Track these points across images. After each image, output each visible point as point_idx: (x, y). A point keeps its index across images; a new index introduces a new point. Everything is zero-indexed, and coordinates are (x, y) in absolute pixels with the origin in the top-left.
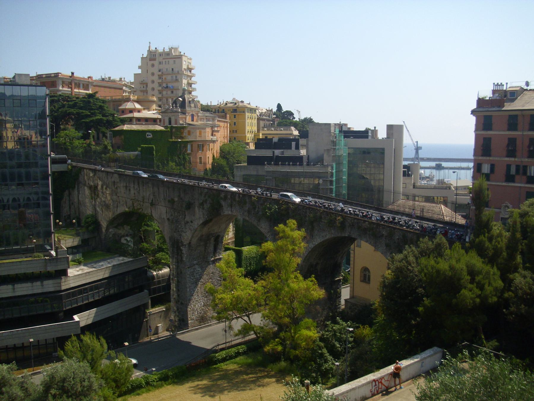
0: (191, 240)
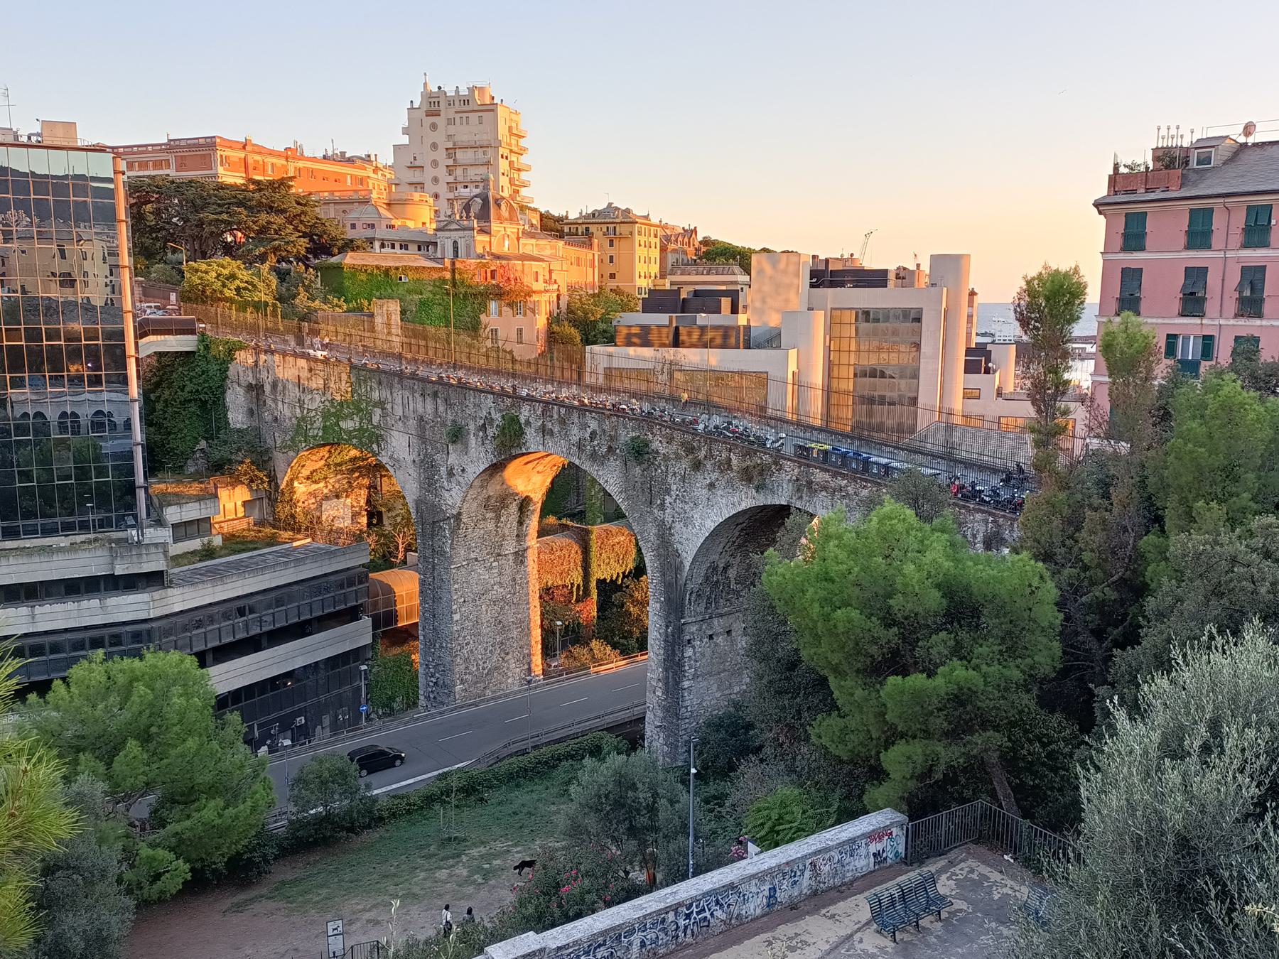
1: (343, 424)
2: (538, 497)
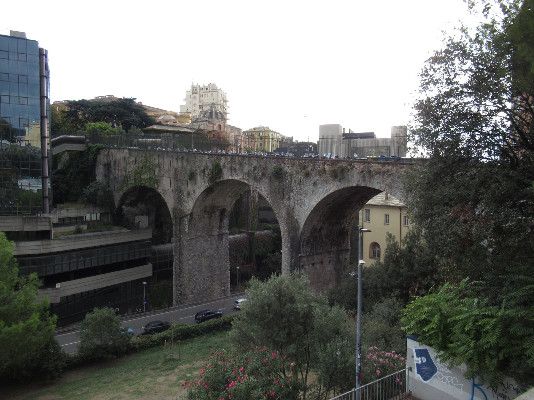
0: (192, 210)
1: (143, 177)
2: (229, 209)
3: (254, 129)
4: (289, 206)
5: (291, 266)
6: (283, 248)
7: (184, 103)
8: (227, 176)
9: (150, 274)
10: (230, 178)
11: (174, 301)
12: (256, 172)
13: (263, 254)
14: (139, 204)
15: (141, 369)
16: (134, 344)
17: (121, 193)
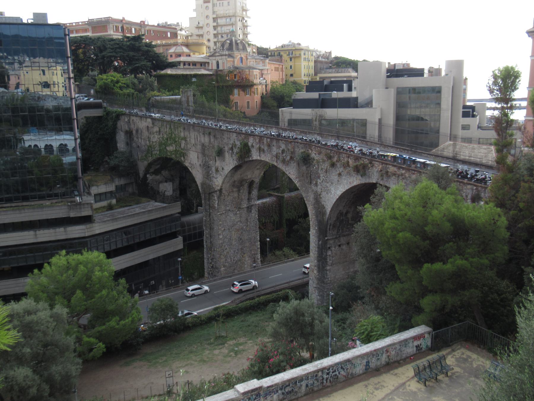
0: (221, 186)
1: (168, 148)
2: (257, 180)
3: (282, 46)
4: (317, 191)
5: (318, 248)
6: (311, 230)
7: (194, 15)
8: (255, 156)
9: (181, 247)
10: (259, 158)
11: (206, 273)
12: (284, 155)
13: (294, 217)
14: (163, 172)
15: (199, 344)
16: (188, 323)
17: (146, 163)
